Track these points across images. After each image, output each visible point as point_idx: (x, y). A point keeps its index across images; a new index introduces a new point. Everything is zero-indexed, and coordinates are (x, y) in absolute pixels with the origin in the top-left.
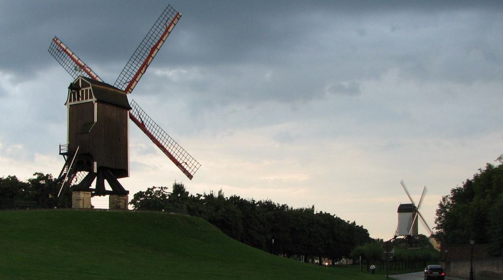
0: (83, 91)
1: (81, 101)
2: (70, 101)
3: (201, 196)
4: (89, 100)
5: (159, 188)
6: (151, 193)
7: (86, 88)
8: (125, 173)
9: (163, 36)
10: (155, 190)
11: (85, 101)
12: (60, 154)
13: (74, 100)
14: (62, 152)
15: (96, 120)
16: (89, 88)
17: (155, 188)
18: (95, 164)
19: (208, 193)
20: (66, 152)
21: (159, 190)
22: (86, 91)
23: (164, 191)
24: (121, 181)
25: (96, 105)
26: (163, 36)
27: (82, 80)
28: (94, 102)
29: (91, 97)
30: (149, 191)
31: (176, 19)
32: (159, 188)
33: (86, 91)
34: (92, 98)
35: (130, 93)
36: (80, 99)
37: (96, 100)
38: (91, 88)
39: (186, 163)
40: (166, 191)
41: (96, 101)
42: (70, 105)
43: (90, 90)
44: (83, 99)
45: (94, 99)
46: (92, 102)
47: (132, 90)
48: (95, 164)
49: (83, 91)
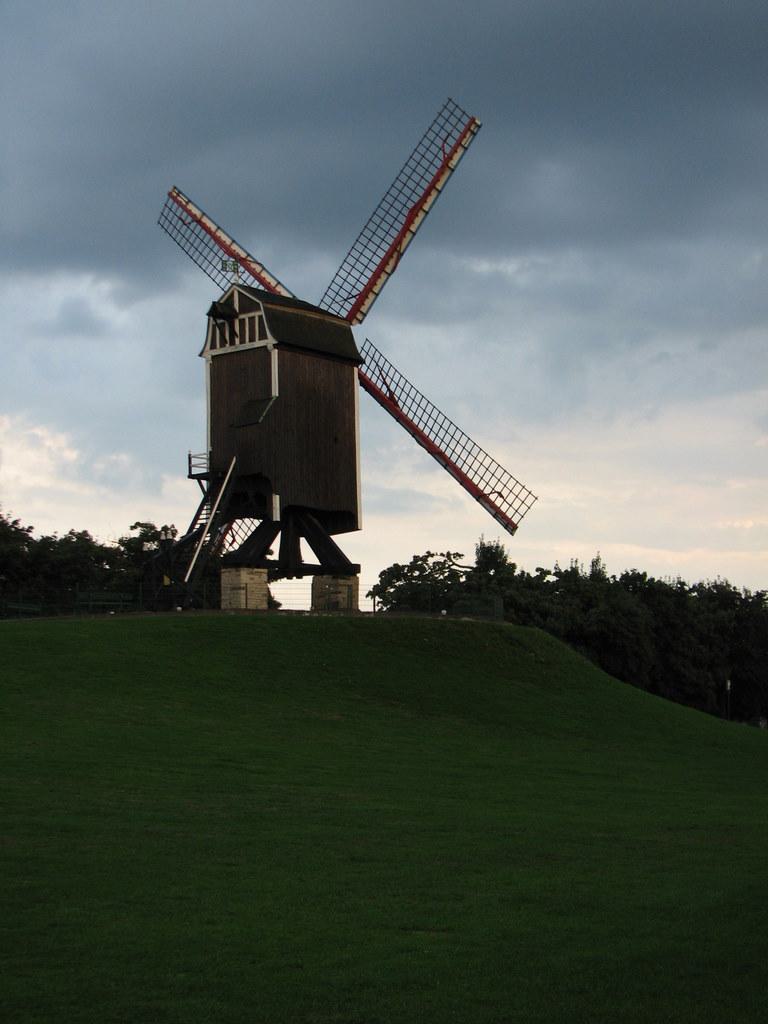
0: (242, 322)
1: (239, 347)
2: (213, 346)
3: (549, 573)
4: (258, 344)
5: (442, 555)
6: (422, 569)
7: (251, 315)
8: (350, 522)
9: (437, 179)
10: (431, 561)
11: (248, 345)
12: (191, 476)
13: (223, 344)
14: (195, 471)
15: (275, 392)
16: (256, 314)
17: (432, 555)
18: (276, 499)
19: (565, 567)
20: (205, 471)
21: (442, 559)
22: (252, 319)
23: (454, 564)
24: (341, 540)
25: (275, 354)
26: (437, 179)
27: (239, 293)
28: (270, 347)
29: (263, 336)
30: (418, 563)
31: (469, 133)
32: (442, 555)
33: (252, 319)
34: (266, 338)
35: (361, 322)
36: (237, 340)
37: (275, 342)
38: (262, 313)
39: (500, 494)
40: (459, 562)
41: (275, 346)
42: (213, 357)
43: (260, 317)
44: (242, 341)
45: (270, 341)
46: (265, 347)
47: (365, 315)
48: (276, 499)
49: (242, 322)
